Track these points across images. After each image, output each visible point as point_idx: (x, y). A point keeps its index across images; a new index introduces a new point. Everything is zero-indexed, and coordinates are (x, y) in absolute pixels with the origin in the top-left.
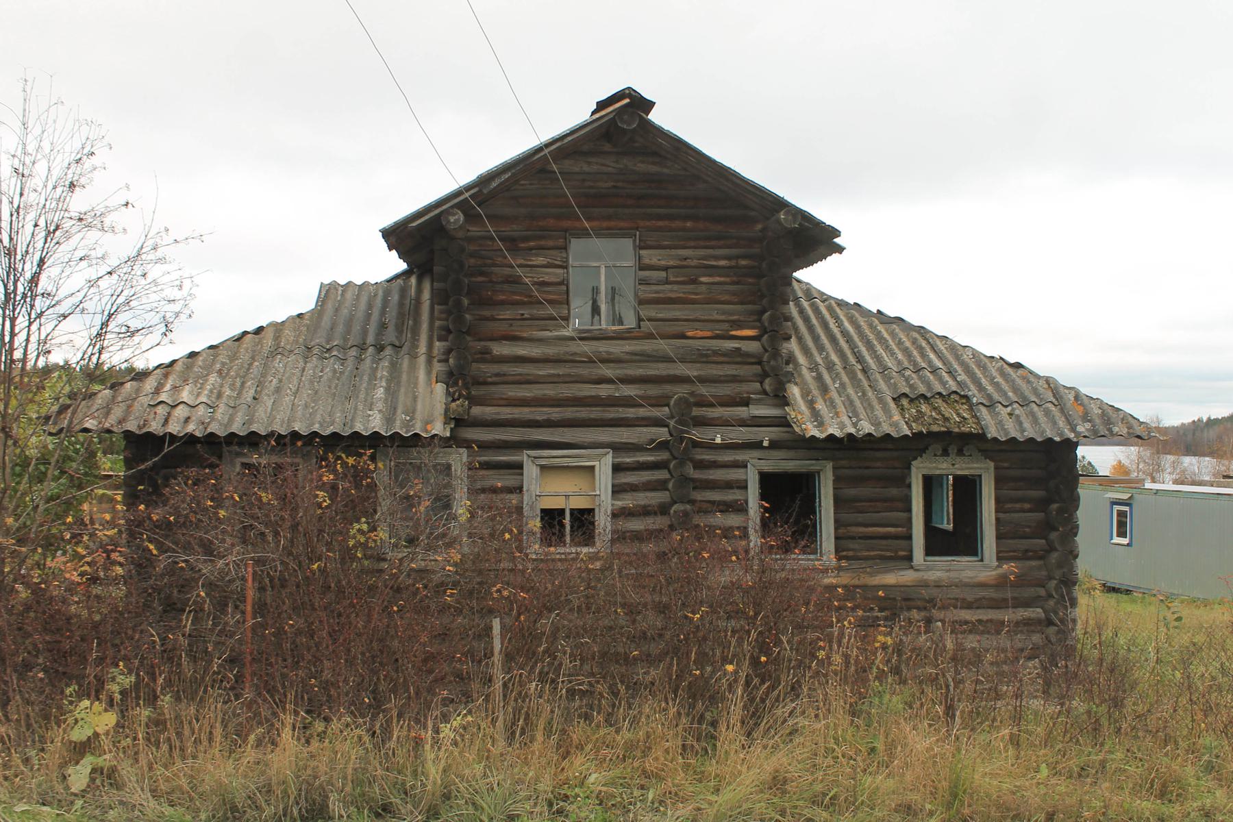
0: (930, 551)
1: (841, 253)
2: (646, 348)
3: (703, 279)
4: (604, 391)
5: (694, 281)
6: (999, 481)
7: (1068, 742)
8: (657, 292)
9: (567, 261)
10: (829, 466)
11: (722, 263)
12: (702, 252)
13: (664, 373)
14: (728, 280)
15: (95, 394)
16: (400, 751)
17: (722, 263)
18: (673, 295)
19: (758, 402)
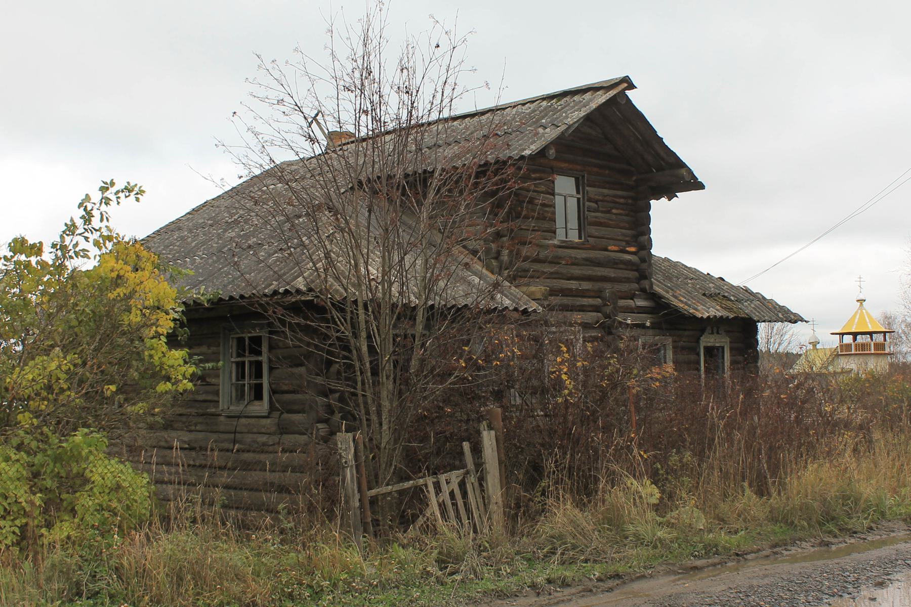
0: (250, 353)
1: (669, 200)
2: (591, 256)
3: (614, 211)
4: (573, 285)
5: (609, 212)
6: (731, 349)
7: (152, 338)
8: (596, 217)
9: (553, 189)
10: (669, 341)
11: (622, 201)
12: (612, 192)
13: (599, 274)
14: (621, 211)
15: (55, 463)
16: (462, 568)
17: (622, 201)
18: (602, 220)
19: (639, 297)
